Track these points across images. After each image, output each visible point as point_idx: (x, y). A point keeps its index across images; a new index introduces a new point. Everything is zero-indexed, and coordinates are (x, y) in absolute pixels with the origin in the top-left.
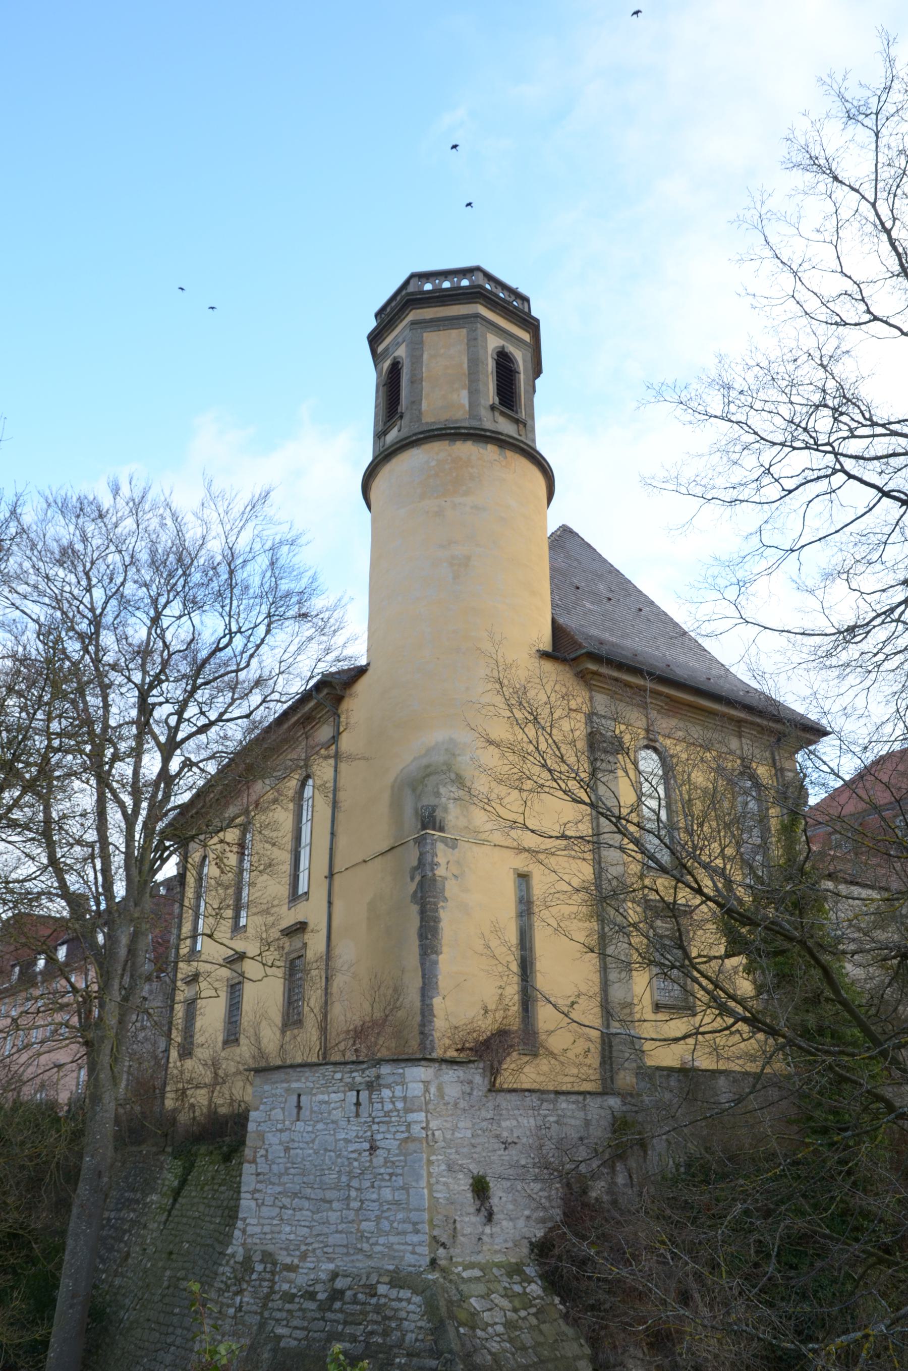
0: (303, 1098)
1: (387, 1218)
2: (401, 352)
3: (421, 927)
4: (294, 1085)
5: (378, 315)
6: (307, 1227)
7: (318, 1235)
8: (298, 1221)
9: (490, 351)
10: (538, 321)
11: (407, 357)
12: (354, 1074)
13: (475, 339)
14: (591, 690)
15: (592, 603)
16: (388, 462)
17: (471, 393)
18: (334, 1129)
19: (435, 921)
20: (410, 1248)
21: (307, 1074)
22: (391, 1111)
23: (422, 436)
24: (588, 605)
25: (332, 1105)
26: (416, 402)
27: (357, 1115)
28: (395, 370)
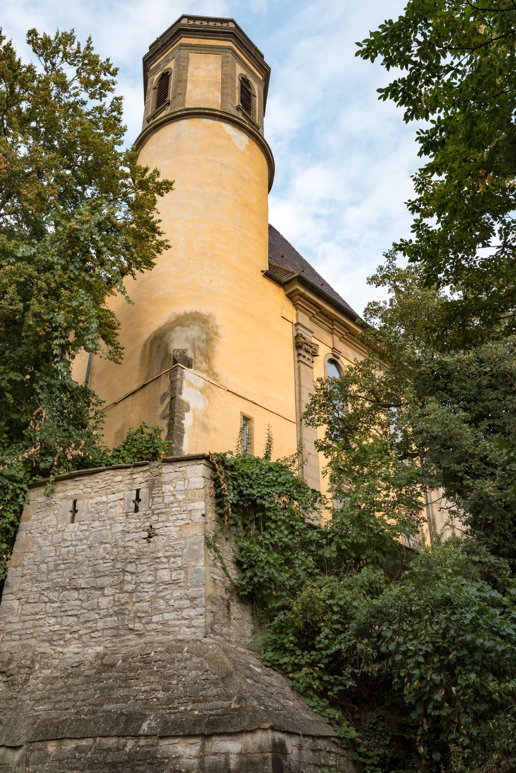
0: (78, 503)
1: (162, 598)
2: (171, 65)
5: (150, 47)
9: (237, 75)
14: (297, 309)
16: (156, 132)
17: (222, 94)
19: (180, 431)
20: (187, 622)
21: (85, 482)
22: (172, 503)
27: (136, 510)
28: (165, 77)
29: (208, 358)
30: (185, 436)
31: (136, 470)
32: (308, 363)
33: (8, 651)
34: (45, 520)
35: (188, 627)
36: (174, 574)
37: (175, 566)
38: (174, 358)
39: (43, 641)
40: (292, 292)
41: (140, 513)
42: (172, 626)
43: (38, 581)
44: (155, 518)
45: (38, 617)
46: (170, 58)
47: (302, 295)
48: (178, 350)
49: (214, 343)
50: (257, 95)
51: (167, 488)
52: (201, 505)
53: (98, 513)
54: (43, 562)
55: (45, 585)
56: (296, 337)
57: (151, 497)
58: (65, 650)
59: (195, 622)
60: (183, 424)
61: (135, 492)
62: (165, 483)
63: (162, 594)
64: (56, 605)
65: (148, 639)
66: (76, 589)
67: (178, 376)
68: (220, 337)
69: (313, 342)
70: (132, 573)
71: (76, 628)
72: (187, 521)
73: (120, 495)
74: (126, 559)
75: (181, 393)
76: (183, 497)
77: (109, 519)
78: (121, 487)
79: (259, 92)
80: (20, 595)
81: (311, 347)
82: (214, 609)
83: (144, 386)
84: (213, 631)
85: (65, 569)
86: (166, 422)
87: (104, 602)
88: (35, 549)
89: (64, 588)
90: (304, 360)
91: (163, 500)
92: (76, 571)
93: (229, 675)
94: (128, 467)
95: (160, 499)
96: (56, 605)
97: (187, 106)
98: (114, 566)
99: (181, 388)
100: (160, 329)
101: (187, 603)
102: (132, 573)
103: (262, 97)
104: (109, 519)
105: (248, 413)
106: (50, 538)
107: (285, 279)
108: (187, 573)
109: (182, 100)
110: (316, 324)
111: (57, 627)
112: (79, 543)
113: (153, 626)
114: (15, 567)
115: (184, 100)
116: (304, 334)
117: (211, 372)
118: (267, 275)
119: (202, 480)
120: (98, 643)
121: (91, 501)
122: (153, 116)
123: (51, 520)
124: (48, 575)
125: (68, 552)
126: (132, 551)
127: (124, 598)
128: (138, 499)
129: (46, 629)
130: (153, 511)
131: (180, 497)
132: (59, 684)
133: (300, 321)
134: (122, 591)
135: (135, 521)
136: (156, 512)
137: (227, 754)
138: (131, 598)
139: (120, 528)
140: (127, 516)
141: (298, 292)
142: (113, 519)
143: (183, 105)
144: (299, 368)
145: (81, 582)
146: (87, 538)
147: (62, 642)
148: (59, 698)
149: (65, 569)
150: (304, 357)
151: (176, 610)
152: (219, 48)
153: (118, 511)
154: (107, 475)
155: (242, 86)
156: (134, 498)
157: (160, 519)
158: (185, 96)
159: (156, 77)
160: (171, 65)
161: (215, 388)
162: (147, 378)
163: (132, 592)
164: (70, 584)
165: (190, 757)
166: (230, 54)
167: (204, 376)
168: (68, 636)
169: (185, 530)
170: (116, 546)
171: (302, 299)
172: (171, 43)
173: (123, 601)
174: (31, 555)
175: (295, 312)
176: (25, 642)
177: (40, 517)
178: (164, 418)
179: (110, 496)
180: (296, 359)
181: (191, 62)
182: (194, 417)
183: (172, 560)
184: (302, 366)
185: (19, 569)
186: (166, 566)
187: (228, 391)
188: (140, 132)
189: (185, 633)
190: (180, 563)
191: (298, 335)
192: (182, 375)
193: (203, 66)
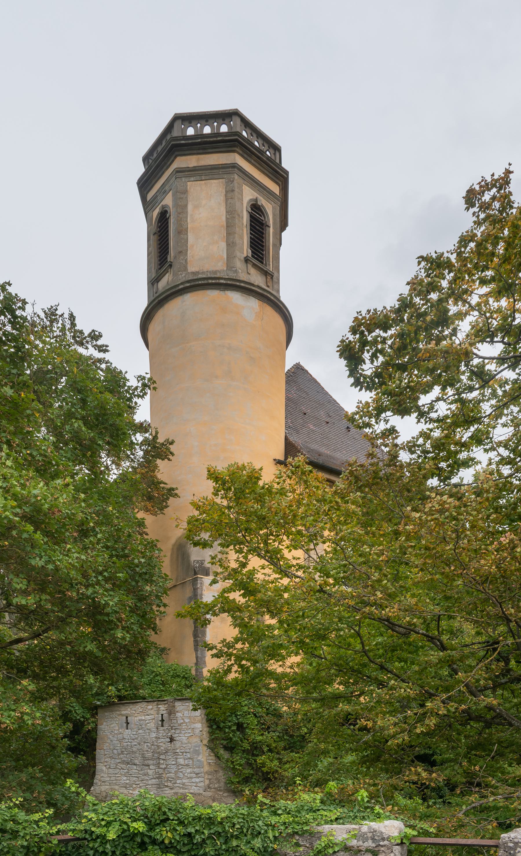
0: (129, 718)
1: (181, 772)
2: (168, 201)
3: (194, 631)
4: (123, 712)
5: (146, 159)
9: (245, 205)
10: (287, 173)
13: (233, 191)
17: (228, 245)
22: (182, 723)
23: (188, 285)
26: (183, 252)
27: (162, 726)
28: (164, 217)
31: (159, 703)
34: (112, 726)
38: (195, 570)
44: (173, 731)
46: (167, 188)
48: (198, 561)
51: (179, 715)
52: (199, 726)
59: (199, 785)
67: (199, 586)
70: (163, 760)
71: (137, 783)
73: (152, 717)
75: (201, 598)
77: (148, 729)
78: (152, 712)
80: (105, 764)
82: (210, 777)
87: (150, 772)
89: (128, 763)
95: (175, 721)
97: (191, 269)
98: (153, 756)
99: (202, 595)
101: (194, 775)
102: (163, 760)
104: (148, 729)
108: (193, 761)
109: (183, 262)
111: (128, 781)
113: (177, 785)
115: (186, 260)
123: (115, 727)
125: (127, 745)
127: (161, 771)
128: (162, 720)
129: (123, 782)
131: (187, 720)
134: (159, 768)
138: (164, 771)
139: (154, 735)
145: (136, 762)
146: (137, 739)
151: (188, 778)
153: (152, 725)
154: (144, 705)
156: (160, 719)
158: (186, 254)
160: (168, 201)
163: (165, 769)
166: (236, 177)
168: (134, 786)
172: (166, 163)
176: (113, 787)
181: (190, 198)
192: (201, 583)
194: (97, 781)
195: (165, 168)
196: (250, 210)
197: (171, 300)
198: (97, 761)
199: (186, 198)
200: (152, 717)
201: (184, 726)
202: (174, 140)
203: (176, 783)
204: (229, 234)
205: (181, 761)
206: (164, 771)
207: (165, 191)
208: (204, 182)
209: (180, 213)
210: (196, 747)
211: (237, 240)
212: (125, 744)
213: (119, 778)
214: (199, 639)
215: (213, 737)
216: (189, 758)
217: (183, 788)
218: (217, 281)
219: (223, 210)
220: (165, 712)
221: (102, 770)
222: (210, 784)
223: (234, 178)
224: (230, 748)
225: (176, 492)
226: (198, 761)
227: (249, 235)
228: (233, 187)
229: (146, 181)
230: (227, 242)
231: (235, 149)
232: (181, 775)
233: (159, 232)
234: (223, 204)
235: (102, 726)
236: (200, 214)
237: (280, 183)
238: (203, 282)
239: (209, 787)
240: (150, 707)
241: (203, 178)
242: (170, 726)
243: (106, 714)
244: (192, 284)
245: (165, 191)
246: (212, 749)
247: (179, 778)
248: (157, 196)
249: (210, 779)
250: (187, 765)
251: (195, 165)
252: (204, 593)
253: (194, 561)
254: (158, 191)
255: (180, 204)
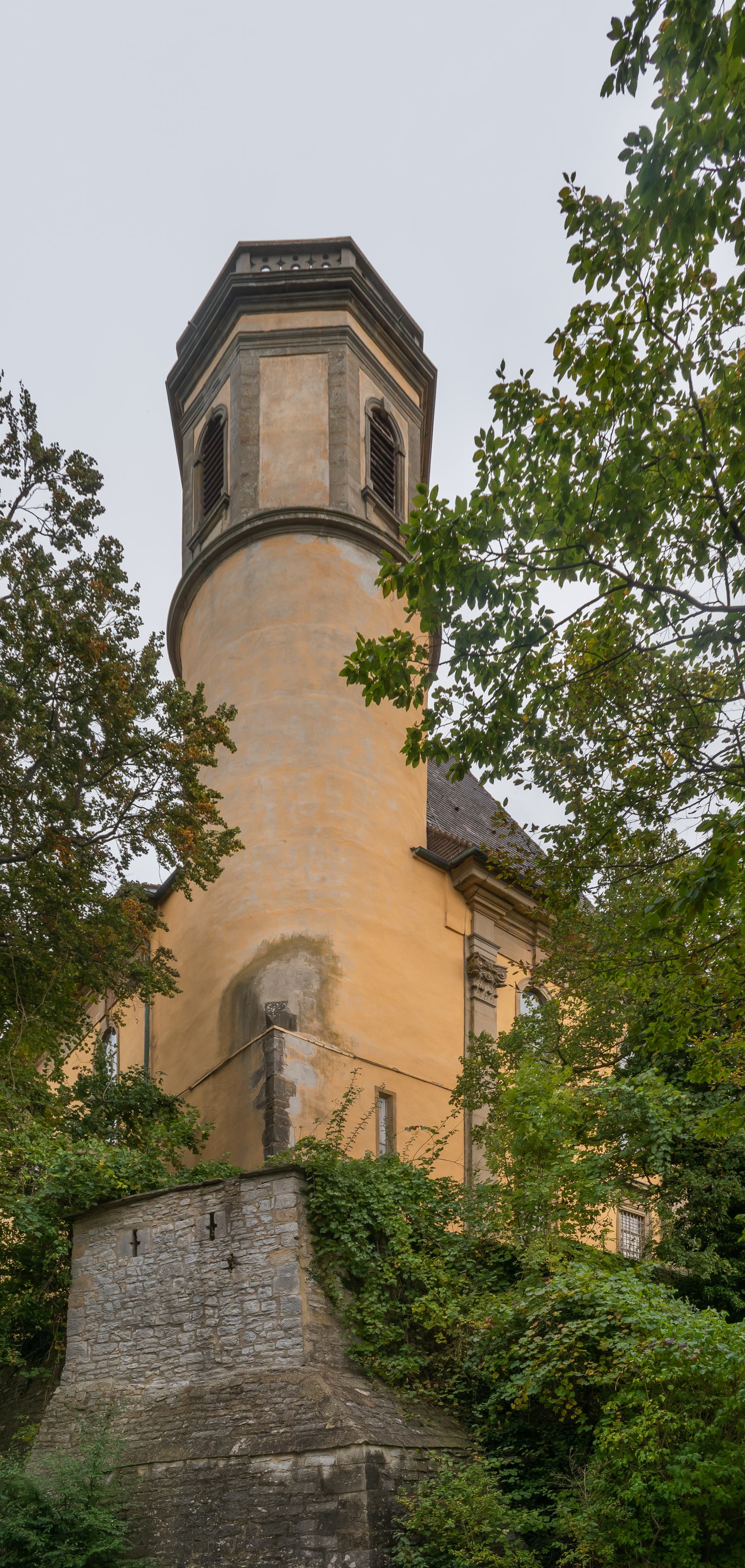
0: (140, 1233)
1: (252, 1330)
2: (224, 397)
3: (266, 1132)
4: (128, 1222)
5: (180, 346)
6: (154, 1353)
7: (167, 1358)
8: (141, 1349)
9: (362, 403)
10: (434, 371)
11: (232, 402)
12: (206, 1198)
13: (342, 373)
14: (472, 910)
15: (472, 829)
16: (208, 575)
17: (332, 463)
18: (182, 1256)
19: (283, 1123)
20: (282, 1352)
21: (144, 1208)
22: (256, 1226)
23: (260, 523)
24: (469, 830)
25: (179, 1233)
26: (250, 475)
27: (212, 1238)
28: (215, 428)
29: (322, 1011)
30: (291, 1129)
31: (206, 1190)
32: (488, 999)
33: (84, 1391)
34: (102, 1255)
35: (284, 1357)
36: (264, 1304)
37: (264, 1296)
38: (267, 1018)
39: (121, 1379)
40: (464, 881)
41: (217, 1241)
42: (265, 1357)
43: (104, 1321)
44: (237, 1244)
45: (111, 1356)
46: (221, 376)
47: (482, 885)
48: (273, 1004)
49: (330, 986)
50: (406, 450)
51: (249, 1209)
52: (292, 1227)
53: (165, 1244)
54: (107, 1301)
55: (115, 1324)
56: (469, 959)
57: (229, 1221)
58: (148, 1386)
59: (291, 1352)
60: (287, 1114)
61: (208, 1216)
62: (245, 1203)
63: (251, 1326)
64: (130, 1343)
65: (238, 1371)
66: (151, 1326)
67: (276, 1045)
68: (341, 975)
69: (498, 964)
70: (213, 1307)
71: (156, 1365)
72: (276, 1247)
73: (190, 1221)
74: (204, 1292)
75: (281, 1070)
76: (270, 1218)
77: (180, 1249)
78: (190, 1211)
79: (411, 440)
80: (87, 1335)
81: (494, 973)
82: (314, 1337)
83: (228, 1062)
84: (313, 1359)
85: (134, 1307)
86: (262, 1112)
87: (184, 1338)
88: (95, 1287)
89: (137, 1327)
90: (482, 996)
91: (245, 1224)
92: (147, 1308)
93: (326, 1399)
94: (197, 1187)
95: (241, 1223)
96: (130, 1343)
97: (266, 503)
98: (191, 1301)
99: (281, 1063)
100: (245, 969)
102: (213, 1307)
103: (418, 451)
104: (180, 1249)
105: (389, 1088)
106: (111, 1274)
107: (453, 858)
110: (507, 931)
111: (135, 1365)
112: (146, 1278)
114: (76, 1307)
115: (256, 489)
116: (481, 952)
117: (328, 1034)
118: (420, 855)
119: (293, 1196)
120: (183, 1378)
121: (154, 1230)
122: (201, 537)
123: (108, 1255)
124: (115, 1313)
125: (135, 1288)
126: (211, 1283)
127: (207, 1332)
128: (212, 1226)
129: (123, 1368)
130: (233, 1237)
131: (266, 1219)
132: (144, 1417)
133: (477, 931)
134: (203, 1326)
135: (210, 1250)
136: (237, 1238)
137: (320, 1467)
138: (215, 1332)
139: (194, 1258)
140: (201, 1245)
141: (475, 881)
142: (184, 1249)
143: (255, 503)
144: (472, 1008)
145: (155, 1319)
147: (142, 1379)
148: (145, 1429)
149: (134, 1307)
150: (481, 990)
151: (268, 1341)
152: (323, 334)
155: (374, 433)
156: (208, 1223)
157: (243, 1246)
158: (256, 479)
159: (199, 430)
160: (224, 397)
161: (334, 1057)
162: (231, 1049)
164: (142, 1322)
165: (282, 1471)
166: (348, 351)
167: (314, 1038)
168: (149, 1373)
169: (274, 1257)
170: (191, 1279)
171: (481, 891)
172: (220, 332)
173: (206, 1336)
174: (92, 1294)
175: (469, 914)
177: (95, 1252)
178: (259, 1107)
179: (177, 1223)
180: (468, 995)
181: (264, 385)
182: (303, 1101)
183: (261, 1290)
184: (477, 1004)
185: (81, 1309)
186: (254, 1297)
187: (355, 1058)
188: (179, 576)
189: (281, 1363)
190: (270, 1293)
191: (472, 955)
192: (280, 1042)
193: (289, 392)
194: (69, 1374)
195: (219, 341)
196: (371, 414)
197: (226, 557)
198: (69, 1333)
199: (258, 383)
200: (190, 1221)
201: (260, 1232)
202: (237, 281)
203: (240, 1354)
204: (333, 445)
205: (253, 1306)
206: (215, 1332)
207: (218, 382)
208: (289, 358)
209: (245, 410)
210: (286, 1271)
211: (348, 454)
212: (130, 1287)
213: (115, 1362)
214: (274, 1144)
215: (321, 1253)
216: (271, 1298)
217: (256, 1364)
218: (314, 516)
219: (324, 406)
220: (217, 1208)
221: (80, 1351)
222: (316, 1351)
223: (344, 353)
224: (354, 1284)
225: (237, 837)
226: (290, 1301)
227: (369, 458)
228: (343, 366)
229: (183, 375)
230: (330, 459)
231: (347, 302)
232: (252, 1336)
233: (205, 459)
234: (324, 396)
235: (83, 1259)
236: (282, 411)
237: (422, 390)
238: (287, 517)
239: (313, 1359)
240: (186, 1201)
241: (288, 351)
242: (228, 1234)
243: (91, 1232)
244: (267, 520)
245: (218, 382)
246: (320, 1280)
247: (248, 1343)
248: (202, 397)
249: (315, 1342)
250: (266, 1314)
251: (275, 327)
252: (286, 1060)
253: (267, 1005)
254: (205, 386)
255: (245, 393)
